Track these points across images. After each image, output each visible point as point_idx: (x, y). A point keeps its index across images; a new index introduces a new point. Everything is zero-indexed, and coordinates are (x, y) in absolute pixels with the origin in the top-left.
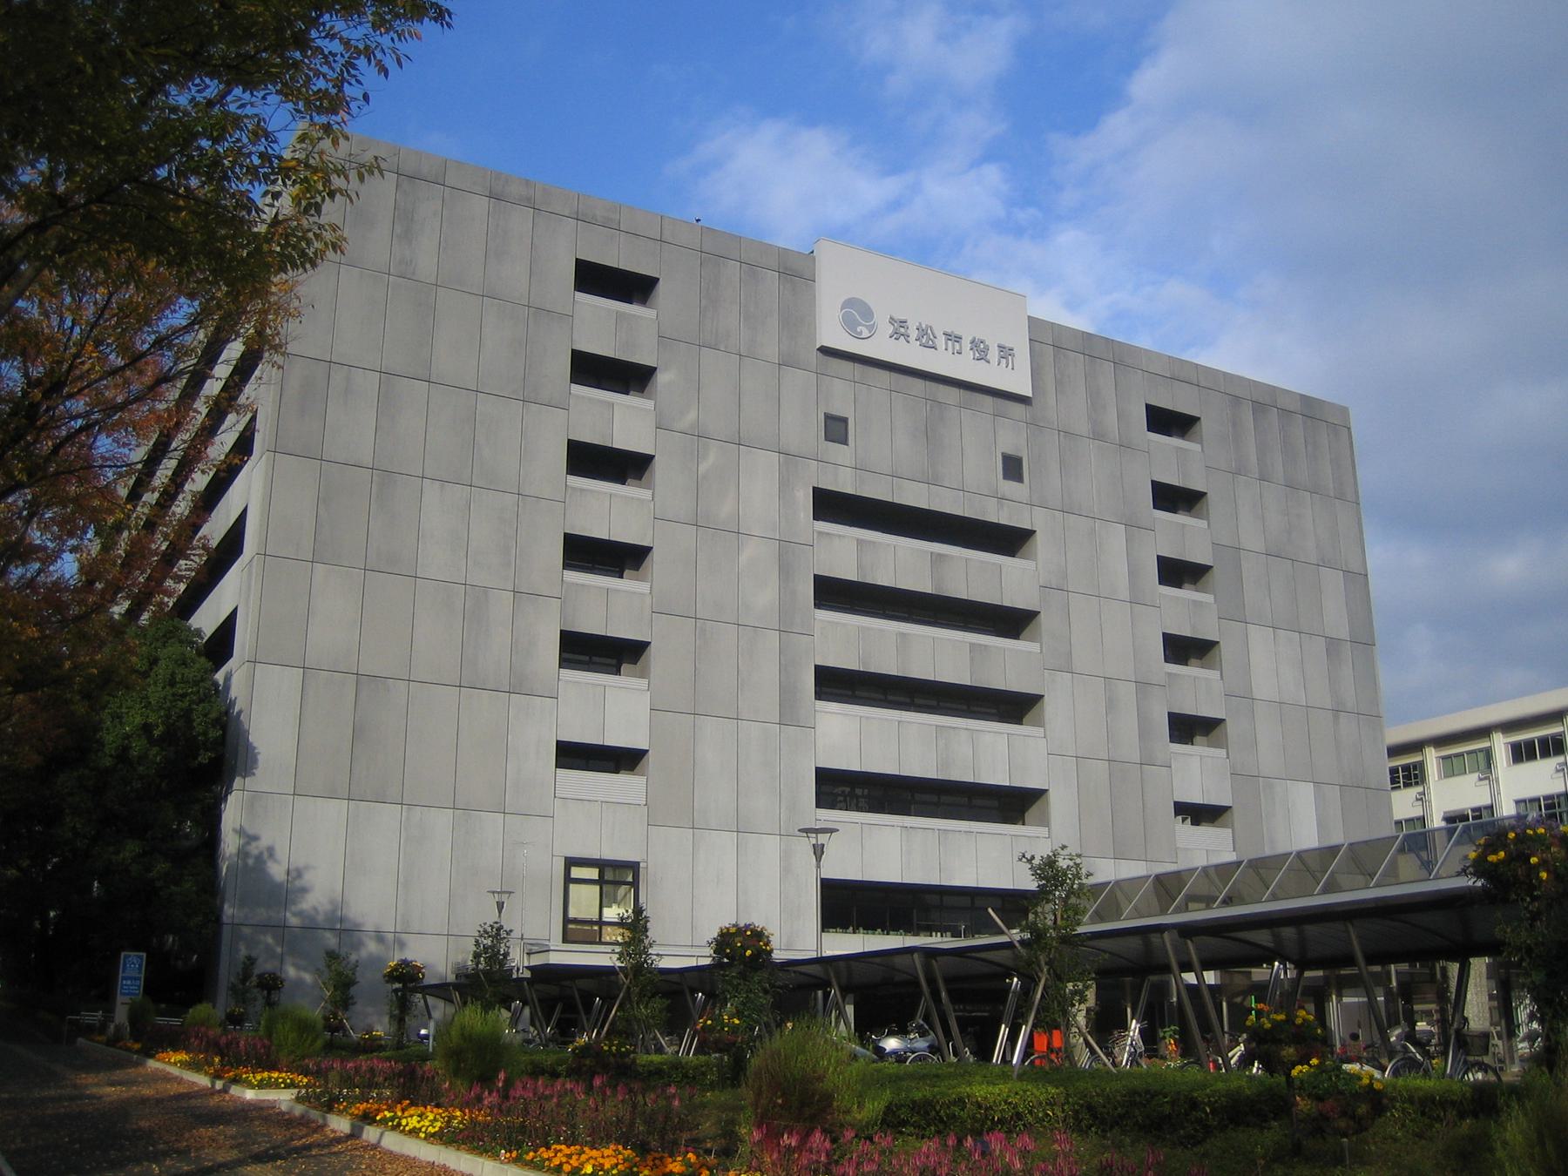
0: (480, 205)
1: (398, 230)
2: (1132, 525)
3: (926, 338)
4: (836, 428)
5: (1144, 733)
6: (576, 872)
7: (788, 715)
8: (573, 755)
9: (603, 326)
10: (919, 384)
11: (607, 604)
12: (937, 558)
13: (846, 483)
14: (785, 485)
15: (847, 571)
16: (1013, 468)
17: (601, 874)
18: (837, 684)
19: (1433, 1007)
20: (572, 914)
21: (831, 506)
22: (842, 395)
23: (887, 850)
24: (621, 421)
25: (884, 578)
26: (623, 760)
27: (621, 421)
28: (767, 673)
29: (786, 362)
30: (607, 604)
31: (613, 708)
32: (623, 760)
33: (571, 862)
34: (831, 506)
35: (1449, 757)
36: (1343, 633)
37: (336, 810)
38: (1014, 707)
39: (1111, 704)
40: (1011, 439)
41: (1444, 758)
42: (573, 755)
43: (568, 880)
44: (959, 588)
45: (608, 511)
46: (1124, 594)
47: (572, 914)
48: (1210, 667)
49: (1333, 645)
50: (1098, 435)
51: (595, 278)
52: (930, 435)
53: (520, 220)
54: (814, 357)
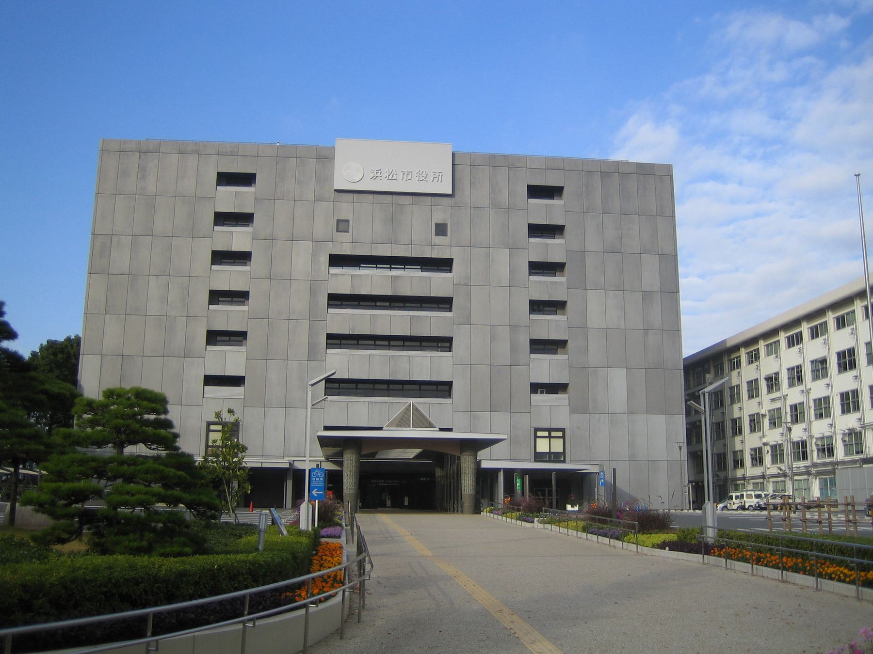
0: (176, 156)
1: (140, 176)
2: (513, 248)
3: (391, 178)
4: (342, 225)
5: (514, 348)
6: (539, 434)
7: (312, 354)
8: (211, 380)
9: (230, 199)
10: (390, 197)
11: (228, 316)
12: (394, 278)
13: (346, 250)
14: (314, 255)
15: (345, 289)
16: (441, 230)
17: (550, 434)
18: (336, 340)
19: (21, 471)
20: (538, 450)
21: (336, 260)
22: (345, 210)
23: (363, 415)
24: (237, 238)
25: (365, 291)
26: (237, 381)
27: (237, 238)
28: (303, 338)
29: (318, 199)
30: (228, 316)
31: (230, 360)
32: (237, 381)
33: (537, 430)
34: (336, 260)
35: (771, 344)
36: (657, 287)
37: (487, 415)
38: (444, 343)
39: (493, 338)
40: (439, 217)
41: (767, 346)
42: (211, 380)
43: (536, 437)
44: (405, 291)
45: (229, 277)
46: (506, 282)
47: (538, 450)
48: (564, 315)
49: (647, 296)
50: (495, 205)
51: (535, 192)
52: (392, 221)
53: (192, 161)
54: (332, 194)
